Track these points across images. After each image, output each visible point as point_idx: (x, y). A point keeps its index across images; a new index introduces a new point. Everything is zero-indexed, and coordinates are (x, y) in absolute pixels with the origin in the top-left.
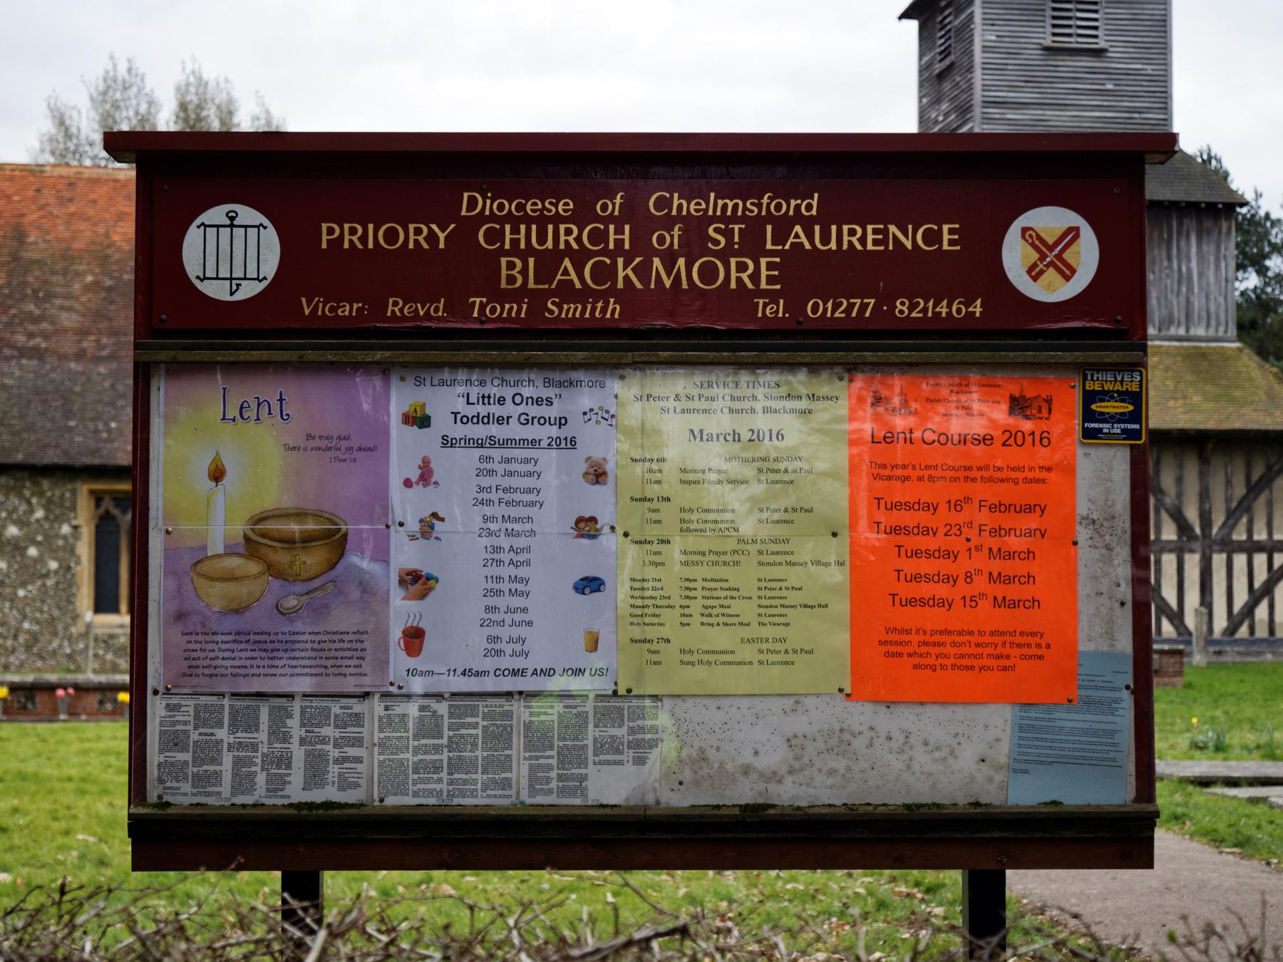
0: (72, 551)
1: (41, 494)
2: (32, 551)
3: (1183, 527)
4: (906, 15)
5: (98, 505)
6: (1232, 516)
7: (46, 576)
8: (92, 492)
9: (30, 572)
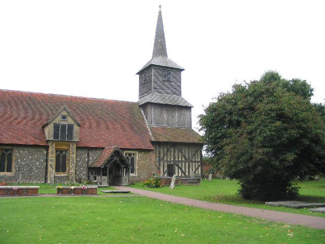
3: (185, 158)
4: (138, 74)
6: (192, 157)
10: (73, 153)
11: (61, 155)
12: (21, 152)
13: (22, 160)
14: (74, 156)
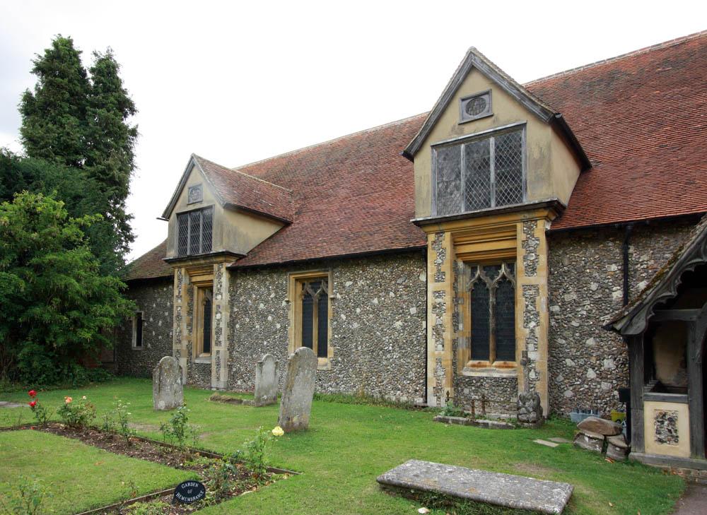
0: (286, 317)
1: (272, 283)
2: (270, 318)
5: (473, 275)
7: (275, 333)
8: (297, 280)
9: (269, 332)
10: (532, 269)
11: (491, 284)
12: (348, 284)
13: (350, 312)
14: (540, 279)
